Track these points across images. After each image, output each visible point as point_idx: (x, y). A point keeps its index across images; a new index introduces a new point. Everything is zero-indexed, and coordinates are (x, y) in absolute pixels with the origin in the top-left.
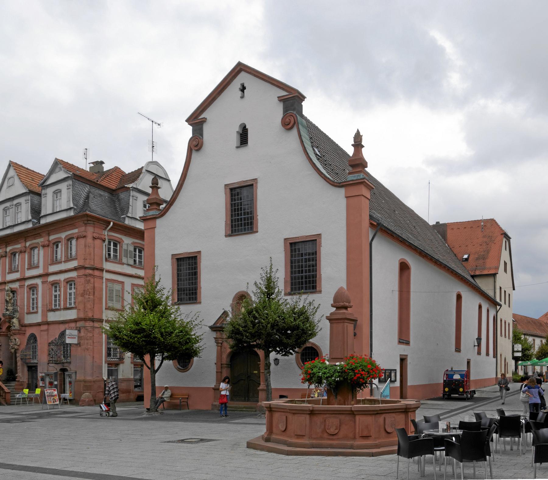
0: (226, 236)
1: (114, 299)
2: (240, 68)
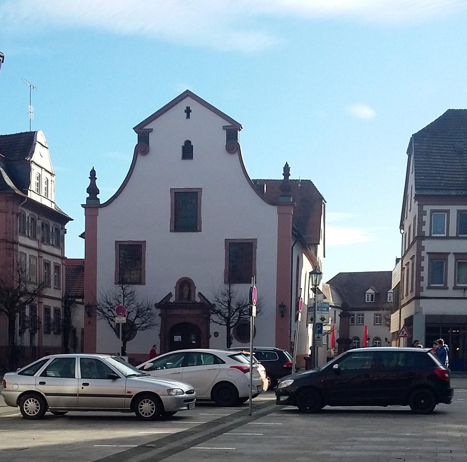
0: (171, 231)
1: (441, 330)
2: (187, 94)
